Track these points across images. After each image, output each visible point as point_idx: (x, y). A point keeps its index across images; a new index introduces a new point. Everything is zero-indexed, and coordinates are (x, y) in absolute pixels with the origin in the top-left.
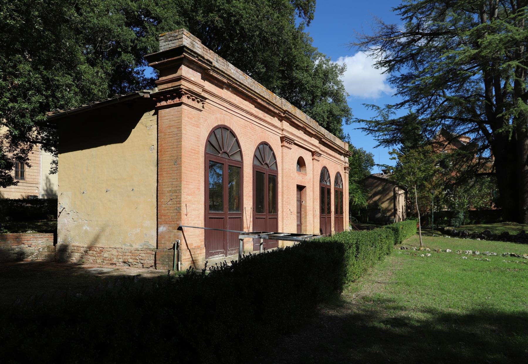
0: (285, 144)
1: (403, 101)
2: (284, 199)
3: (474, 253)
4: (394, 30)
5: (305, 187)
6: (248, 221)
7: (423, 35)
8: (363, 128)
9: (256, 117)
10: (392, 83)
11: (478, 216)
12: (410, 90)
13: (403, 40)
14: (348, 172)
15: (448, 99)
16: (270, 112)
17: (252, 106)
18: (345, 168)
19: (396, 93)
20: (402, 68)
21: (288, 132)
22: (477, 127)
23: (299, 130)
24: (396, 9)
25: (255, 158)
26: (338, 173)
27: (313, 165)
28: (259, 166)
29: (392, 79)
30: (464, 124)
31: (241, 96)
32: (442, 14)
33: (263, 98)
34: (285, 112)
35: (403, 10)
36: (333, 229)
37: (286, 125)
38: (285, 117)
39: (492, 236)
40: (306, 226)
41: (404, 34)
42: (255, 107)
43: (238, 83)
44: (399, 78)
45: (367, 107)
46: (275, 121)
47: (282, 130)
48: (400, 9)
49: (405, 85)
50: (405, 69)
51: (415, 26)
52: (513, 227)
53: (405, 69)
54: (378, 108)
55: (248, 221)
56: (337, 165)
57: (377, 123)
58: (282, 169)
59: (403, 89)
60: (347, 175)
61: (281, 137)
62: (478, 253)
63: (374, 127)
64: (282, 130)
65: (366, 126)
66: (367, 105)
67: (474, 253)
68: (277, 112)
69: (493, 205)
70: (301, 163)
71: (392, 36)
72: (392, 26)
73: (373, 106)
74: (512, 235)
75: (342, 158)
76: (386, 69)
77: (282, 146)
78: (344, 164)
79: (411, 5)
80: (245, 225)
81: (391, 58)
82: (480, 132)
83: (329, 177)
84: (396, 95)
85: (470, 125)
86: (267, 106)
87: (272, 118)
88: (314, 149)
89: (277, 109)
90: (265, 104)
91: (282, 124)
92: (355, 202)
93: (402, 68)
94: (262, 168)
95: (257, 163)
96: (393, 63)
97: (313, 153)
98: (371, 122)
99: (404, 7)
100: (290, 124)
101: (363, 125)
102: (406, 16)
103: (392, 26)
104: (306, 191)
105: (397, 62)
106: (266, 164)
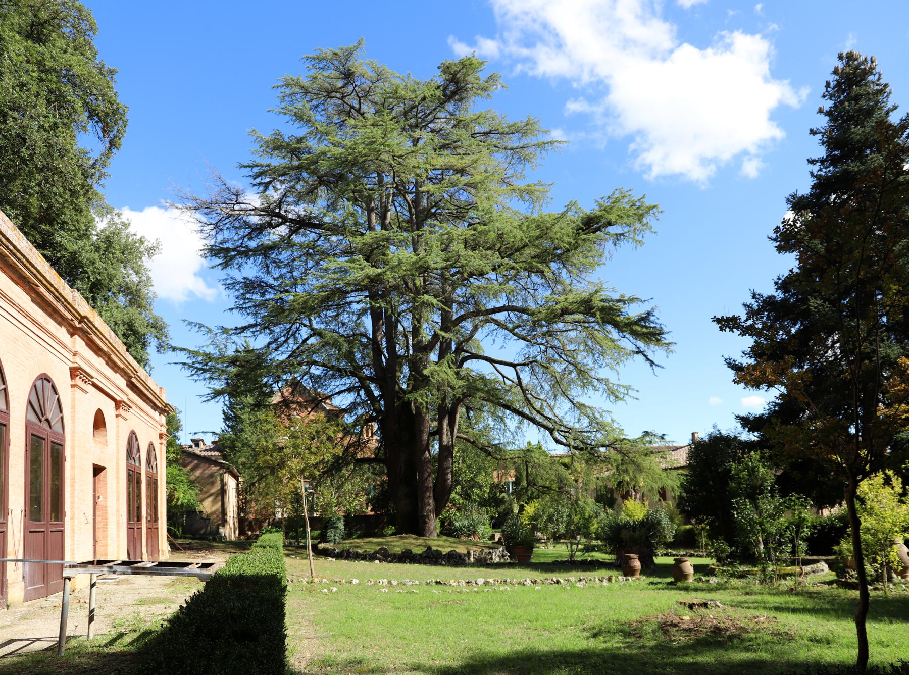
0: (78, 381)
1: (247, 324)
2: (76, 494)
3: (390, 582)
4: (241, 200)
5: (104, 468)
6: (17, 539)
7: (285, 220)
8: (184, 364)
9: (34, 321)
10: (228, 288)
11: (358, 525)
12: (255, 306)
13: (255, 219)
14: (165, 442)
15: (315, 333)
16: (56, 316)
17: (27, 298)
18: (161, 436)
19: (233, 306)
20: (245, 265)
21: (84, 359)
22: (357, 384)
23: (99, 356)
24: (245, 167)
25: (30, 407)
26: (151, 444)
27: (118, 427)
28: (36, 424)
29: (229, 281)
30: (341, 377)
31: (11, 274)
32: (312, 192)
33: (49, 286)
34: (83, 319)
35: (256, 170)
36: (144, 550)
37: (79, 344)
38: (81, 329)
39: (389, 556)
40: (106, 546)
41: (255, 209)
42: (32, 301)
43: (11, 247)
44: (239, 283)
45: (189, 327)
46: (62, 332)
47: (75, 355)
48: (252, 167)
49: (248, 296)
50: (250, 269)
51: (275, 202)
52: (413, 541)
53: (250, 269)
54: (210, 331)
55: (17, 539)
56: (149, 428)
57: (209, 357)
58: (73, 432)
59: (245, 303)
60: (164, 449)
61: (70, 368)
62: (395, 583)
63: (203, 365)
64: (75, 355)
65: (190, 361)
66: (190, 323)
67: (390, 582)
68: (70, 317)
69: (369, 509)
70: (99, 422)
71: (236, 207)
72: (238, 192)
73: (201, 326)
74: (416, 555)
75: (156, 414)
76: (221, 261)
77: (72, 386)
78: (159, 427)
79: (268, 165)
80: (10, 548)
81: (229, 245)
82: (362, 393)
83: (139, 451)
84: (231, 309)
85: (348, 381)
86: (55, 302)
87: (58, 326)
88: (119, 396)
89: (69, 311)
90: (49, 297)
91: (74, 342)
92: (178, 499)
93: (245, 265)
94: (40, 427)
95: (33, 418)
96: (233, 253)
97: (118, 404)
98: (195, 354)
99: (257, 166)
100: (87, 344)
101: (183, 357)
102: (258, 180)
103: (238, 192)
104: (105, 477)
105: (240, 253)
106: (47, 420)
